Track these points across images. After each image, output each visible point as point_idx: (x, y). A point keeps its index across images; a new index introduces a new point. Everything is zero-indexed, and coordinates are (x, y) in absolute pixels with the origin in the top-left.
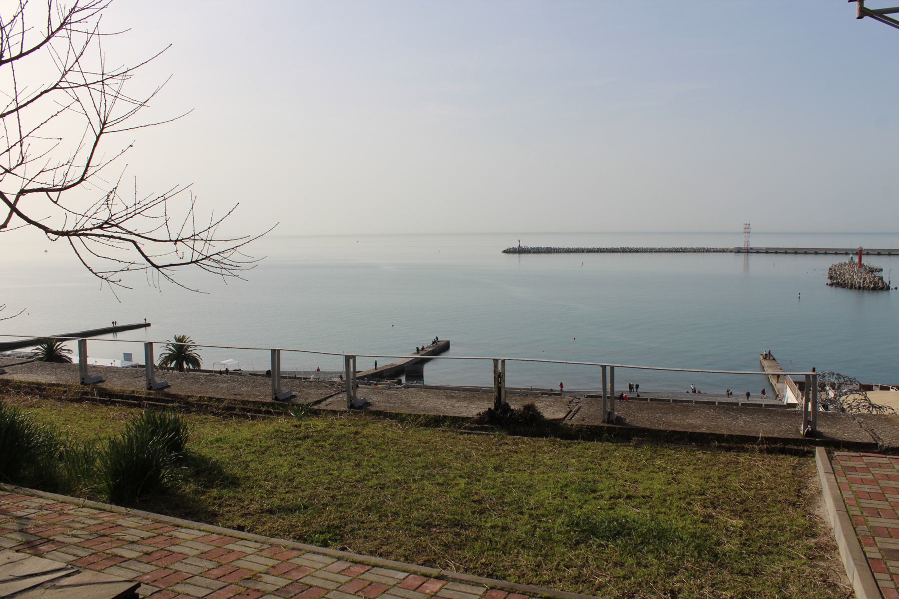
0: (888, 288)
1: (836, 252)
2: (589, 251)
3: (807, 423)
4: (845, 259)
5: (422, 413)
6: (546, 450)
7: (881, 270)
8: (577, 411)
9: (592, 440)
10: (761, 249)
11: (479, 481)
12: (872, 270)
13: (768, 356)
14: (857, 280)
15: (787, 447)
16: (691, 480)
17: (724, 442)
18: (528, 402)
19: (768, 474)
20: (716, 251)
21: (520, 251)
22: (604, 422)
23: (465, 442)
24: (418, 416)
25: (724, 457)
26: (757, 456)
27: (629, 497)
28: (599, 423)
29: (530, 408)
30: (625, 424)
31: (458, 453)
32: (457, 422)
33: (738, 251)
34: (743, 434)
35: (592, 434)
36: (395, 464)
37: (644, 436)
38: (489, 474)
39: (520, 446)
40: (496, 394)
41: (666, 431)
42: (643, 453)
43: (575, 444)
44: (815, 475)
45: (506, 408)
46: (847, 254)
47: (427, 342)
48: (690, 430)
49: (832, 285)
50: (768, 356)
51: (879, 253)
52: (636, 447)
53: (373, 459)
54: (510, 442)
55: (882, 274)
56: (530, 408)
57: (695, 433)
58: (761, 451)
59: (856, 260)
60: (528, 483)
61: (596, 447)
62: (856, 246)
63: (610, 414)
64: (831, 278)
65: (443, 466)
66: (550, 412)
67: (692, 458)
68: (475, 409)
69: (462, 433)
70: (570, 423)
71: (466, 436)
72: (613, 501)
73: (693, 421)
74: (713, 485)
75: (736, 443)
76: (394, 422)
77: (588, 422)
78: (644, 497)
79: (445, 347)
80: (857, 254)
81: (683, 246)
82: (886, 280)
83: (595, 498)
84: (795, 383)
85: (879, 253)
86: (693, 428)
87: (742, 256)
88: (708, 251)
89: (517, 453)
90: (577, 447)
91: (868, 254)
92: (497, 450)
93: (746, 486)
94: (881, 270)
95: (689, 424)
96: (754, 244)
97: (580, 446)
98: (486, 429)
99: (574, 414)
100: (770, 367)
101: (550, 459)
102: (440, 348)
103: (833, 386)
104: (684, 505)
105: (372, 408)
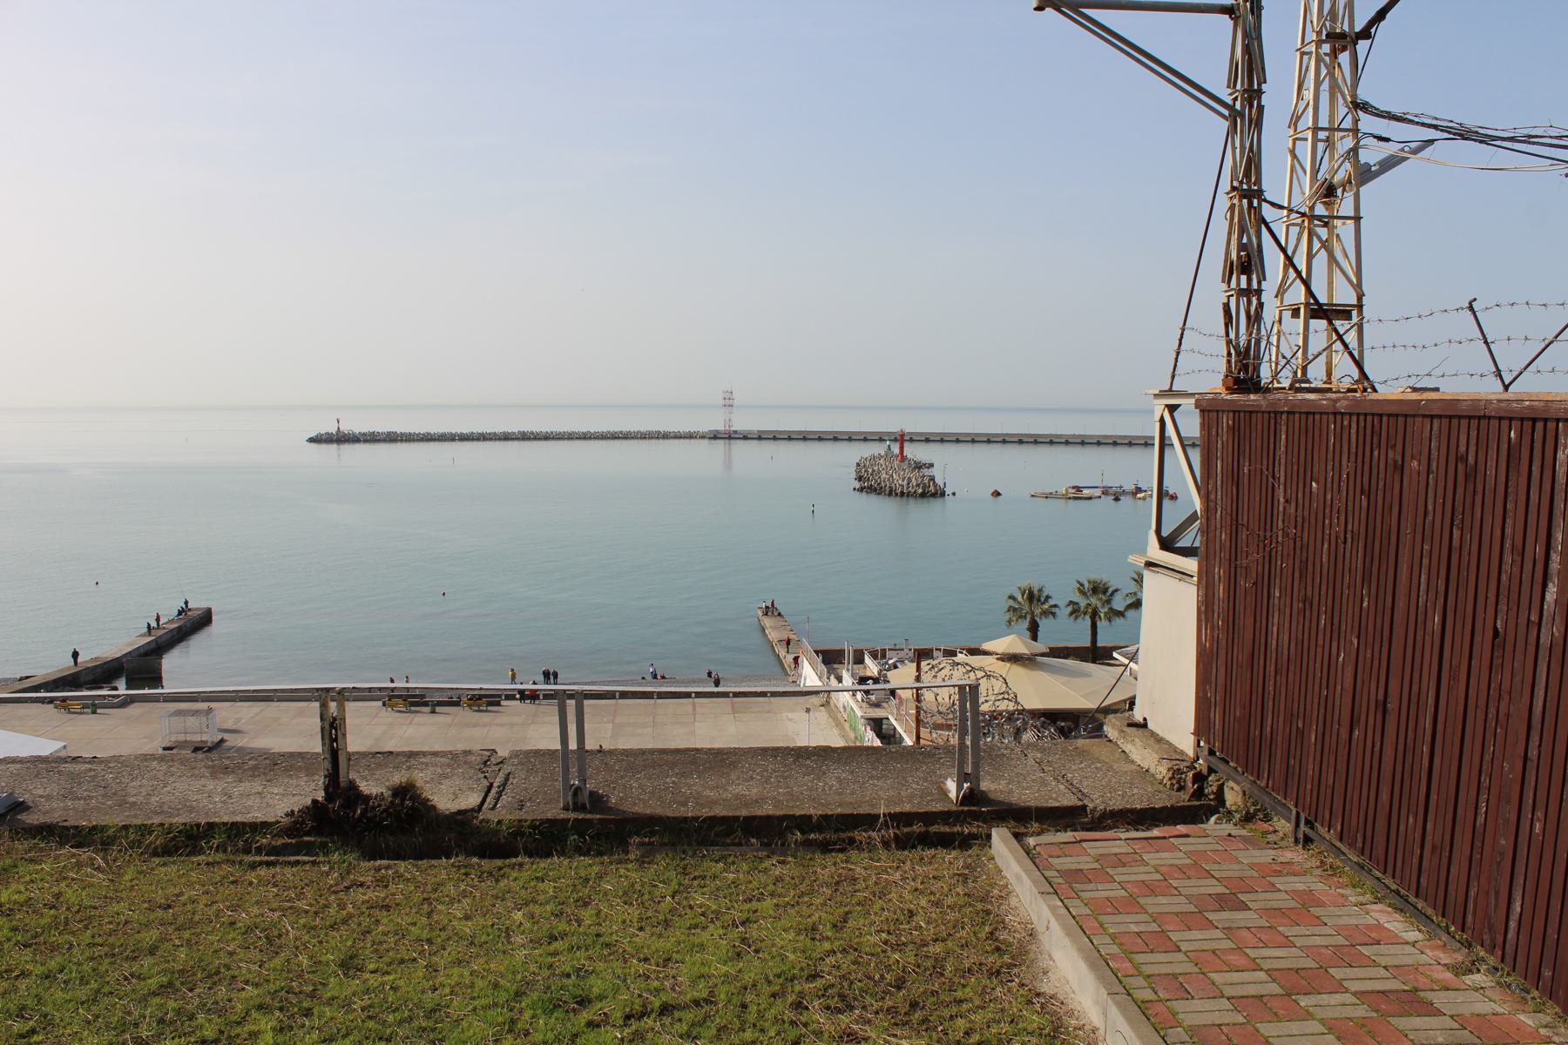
0: (943, 494)
1: (865, 438)
2: (464, 438)
3: (963, 777)
4: (878, 449)
5: (157, 820)
6: (450, 888)
7: (931, 465)
8: (504, 785)
9: (549, 855)
10: (750, 432)
11: (308, 1013)
12: (919, 466)
13: (770, 610)
14: (899, 482)
15: (934, 829)
16: (782, 939)
17: (812, 831)
18: (398, 778)
19: (923, 902)
20: (678, 436)
21: (341, 439)
22: (566, 808)
23: (266, 892)
24: (145, 830)
25: (826, 867)
26: (885, 858)
27: (665, 1009)
28: (555, 812)
29: (405, 792)
30: (610, 809)
31: (248, 930)
32: (240, 837)
33: (715, 436)
34: (848, 811)
35: (544, 839)
36: (83, 993)
37: (653, 833)
38: (334, 987)
39: (392, 888)
40: (327, 764)
41: (696, 819)
42: (663, 871)
43: (512, 867)
44: (1006, 893)
45: (352, 795)
46: (881, 440)
47: (169, 612)
48: (744, 813)
49: (861, 490)
50: (770, 610)
51: (927, 439)
52: (641, 862)
53: (23, 985)
54: (368, 879)
55: (934, 472)
56: (405, 792)
57: (755, 817)
58: (886, 844)
59: (896, 449)
60: (430, 999)
61: (562, 871)
62: (894, 427)
63: (577, 791)
64: (860, 479)
65: (214, 977)
66: (450, 796)
67: (763, 878)
68: (282, 800)
69: (253, 866)
70: (494, 817)
71: (262, 872)
72: (635, 1025)
73: (740, 789)
74: (827, 946)
75: (836, 831)
76: (85, 854)
77: (532, 813)
78: (697, 1003)
79: (205, 619)
80: (896, 440)
81: (625, 429)
82: (939, 481)
83: (591, 1025)
84: (817, 652)
85: (927, 439)
86: (746, 805)
87: (720, 445)
88: (665, 436)
89: (387, 908)
90: (523, 874)
91: (911, 440)
92: (342, 906)
93: (893, 939)
94: (931, 465)
95: (737, 797)
96: (740, 425)
97: (525, 875)
98: (308, 849)
99: (500, 794)
100: (774, 628)
101: (467, 918)
102: (194, 623)
103: (874, 655)
104: (789, 1015)
105: (30, 819)
